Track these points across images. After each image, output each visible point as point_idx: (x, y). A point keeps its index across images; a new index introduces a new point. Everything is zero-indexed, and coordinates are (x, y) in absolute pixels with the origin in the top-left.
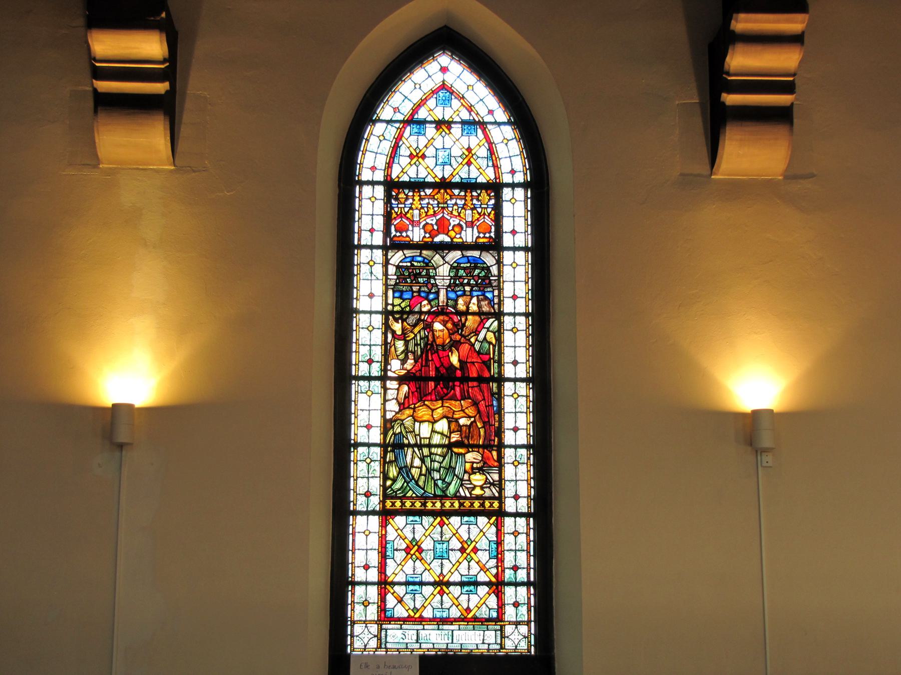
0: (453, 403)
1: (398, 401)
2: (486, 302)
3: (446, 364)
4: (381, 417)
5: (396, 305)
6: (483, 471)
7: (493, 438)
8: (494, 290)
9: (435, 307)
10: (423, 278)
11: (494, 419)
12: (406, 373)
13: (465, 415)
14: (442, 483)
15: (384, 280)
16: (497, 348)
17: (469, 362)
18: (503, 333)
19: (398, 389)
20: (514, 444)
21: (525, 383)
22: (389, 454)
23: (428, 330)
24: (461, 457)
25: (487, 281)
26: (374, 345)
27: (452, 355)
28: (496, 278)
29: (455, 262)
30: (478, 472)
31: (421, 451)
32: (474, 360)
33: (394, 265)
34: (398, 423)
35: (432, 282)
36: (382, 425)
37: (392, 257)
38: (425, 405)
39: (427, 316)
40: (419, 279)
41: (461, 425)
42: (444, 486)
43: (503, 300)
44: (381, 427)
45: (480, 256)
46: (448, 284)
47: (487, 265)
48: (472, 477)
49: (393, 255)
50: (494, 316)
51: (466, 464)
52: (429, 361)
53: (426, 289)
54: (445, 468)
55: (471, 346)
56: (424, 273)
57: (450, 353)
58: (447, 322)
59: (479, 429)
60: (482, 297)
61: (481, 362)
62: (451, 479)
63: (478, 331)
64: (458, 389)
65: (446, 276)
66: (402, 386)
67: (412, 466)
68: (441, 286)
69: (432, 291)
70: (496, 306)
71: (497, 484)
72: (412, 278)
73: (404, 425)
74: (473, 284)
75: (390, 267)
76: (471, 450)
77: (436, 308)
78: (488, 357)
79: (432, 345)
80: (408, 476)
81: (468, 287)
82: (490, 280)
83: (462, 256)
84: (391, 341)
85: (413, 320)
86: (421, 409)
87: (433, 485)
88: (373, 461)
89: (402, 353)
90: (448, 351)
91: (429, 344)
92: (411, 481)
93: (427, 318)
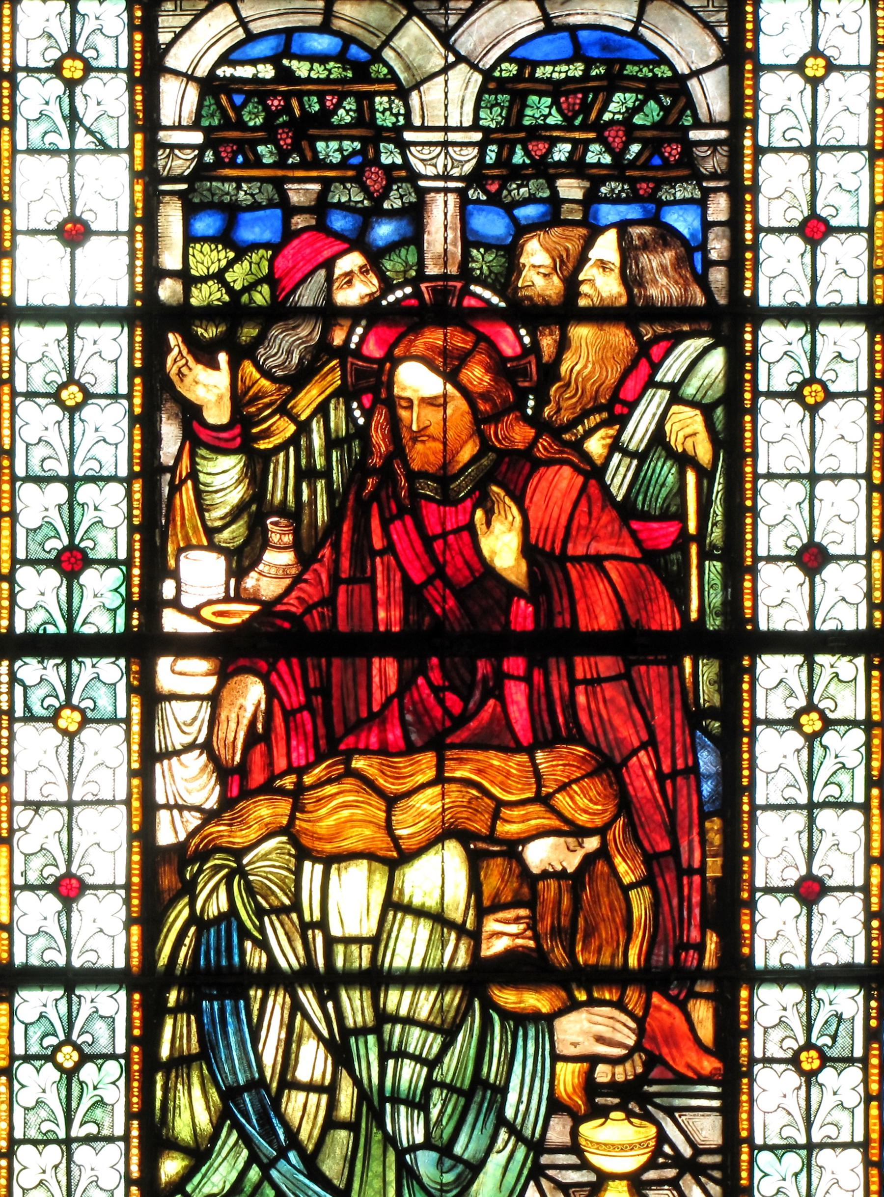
0: (496, 763)
1: (214, 758)
2: (668, 256)
3: (459, 575)
4: (132, 836)
5: (204, 279)
6: (645, 1099)
7: (695, 934)
8: (706, 193)
9: (401, 286)
10: (341, 138)
11: (703, 842)
12: (254, 615)
13: (555, 823)
14: (440, 1162)
15: (138, 152)
16: (718, 487)
17: (577, 560)
18: (754, 411)
19: (214, 699)
20: (799, 963)
21: (860, 661)
22: (169, 1022)
23: (367, 401)
24: (532, 1033)
25: (673, 152)
26: (84, 803)
27: (488, 524)
28: (723, 134)
29: (506, 57)
30: (615, 1108)
31: (330, 1005)
32: (605, 548)
33: (190, 77)
34: (217, 869)
35: (386, 160)
36: (136, 880)
37: (177, 37)
38: (351, 773)
39: (359, 330)
40: (320, 145)
41: (536, 870)
42: (449, 1178)
43: (756, 240)
44: (127, 887)
45: (638, 23)
46: (468, 168)
47: (672, 67)
48: (588, 1130)
49: (186, 29)
50: (705, 327)
51: (560, 1066)
52: (374, 553)
53: (357, 197)
54: (451, 1088)
55: (587, 476)
56: (344, 116)
57: (479, 514)
58: (464, 358)
59: (626, 889)
60: (646, 230)
61: (638, 555)
62: (485, 1142)
63: (625, 403)
64: (517, 694)
65: (460, 129)
66: (233, 682)
67: (288, 1083)
68: (436, 178)
69: (386, 205)
70: (718, 277)
71: (714, 1166)
72: (286, 141)
73: (244, 875)
74: (599, 165)
75: (169, 87)
76: (582, 996)
77: (408, 290)
78: (673, 529)
79: (386, 473)
80: (269, 1133)
81: (573, 182)
82: (689, 146)
83: (541, 26)
84: (178, 458)
85: (289, 352)
86: (333, 796)
87: (391, 1176)
88: (92, 1058)
89: (234, 515)
90: (468, 503)
91: (373, 471)
92: (282, 1154)
93: (363, 339)
